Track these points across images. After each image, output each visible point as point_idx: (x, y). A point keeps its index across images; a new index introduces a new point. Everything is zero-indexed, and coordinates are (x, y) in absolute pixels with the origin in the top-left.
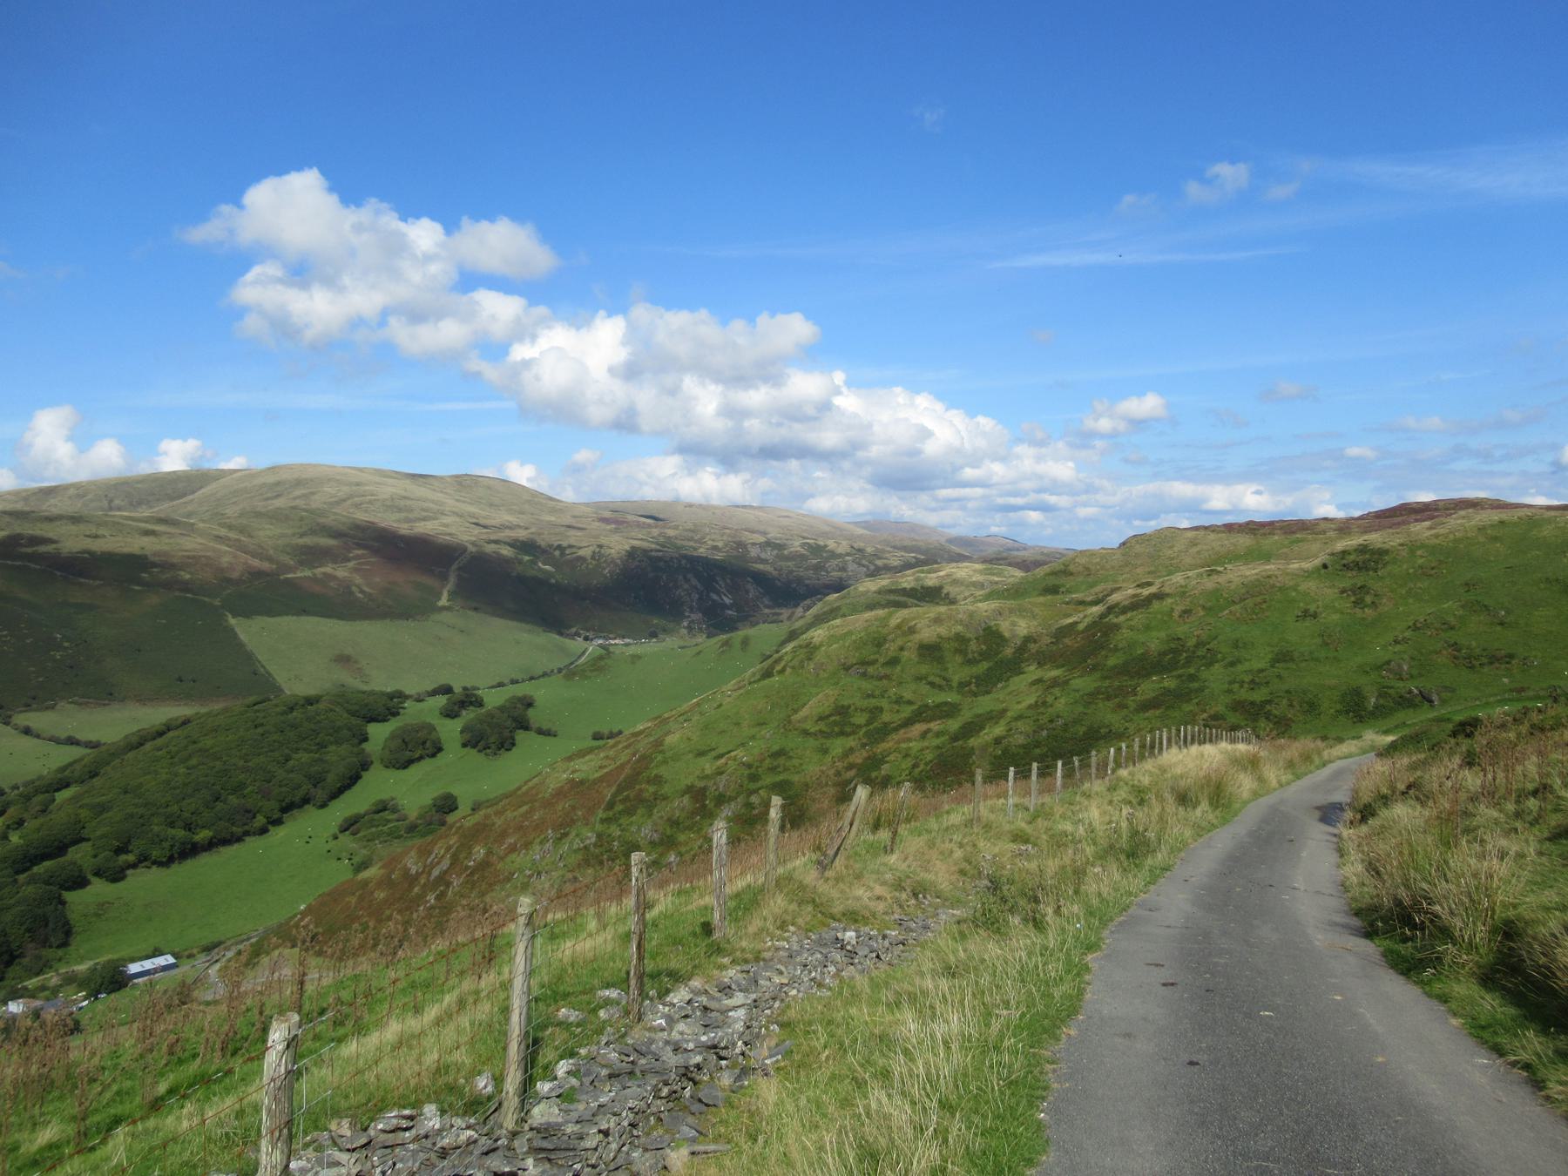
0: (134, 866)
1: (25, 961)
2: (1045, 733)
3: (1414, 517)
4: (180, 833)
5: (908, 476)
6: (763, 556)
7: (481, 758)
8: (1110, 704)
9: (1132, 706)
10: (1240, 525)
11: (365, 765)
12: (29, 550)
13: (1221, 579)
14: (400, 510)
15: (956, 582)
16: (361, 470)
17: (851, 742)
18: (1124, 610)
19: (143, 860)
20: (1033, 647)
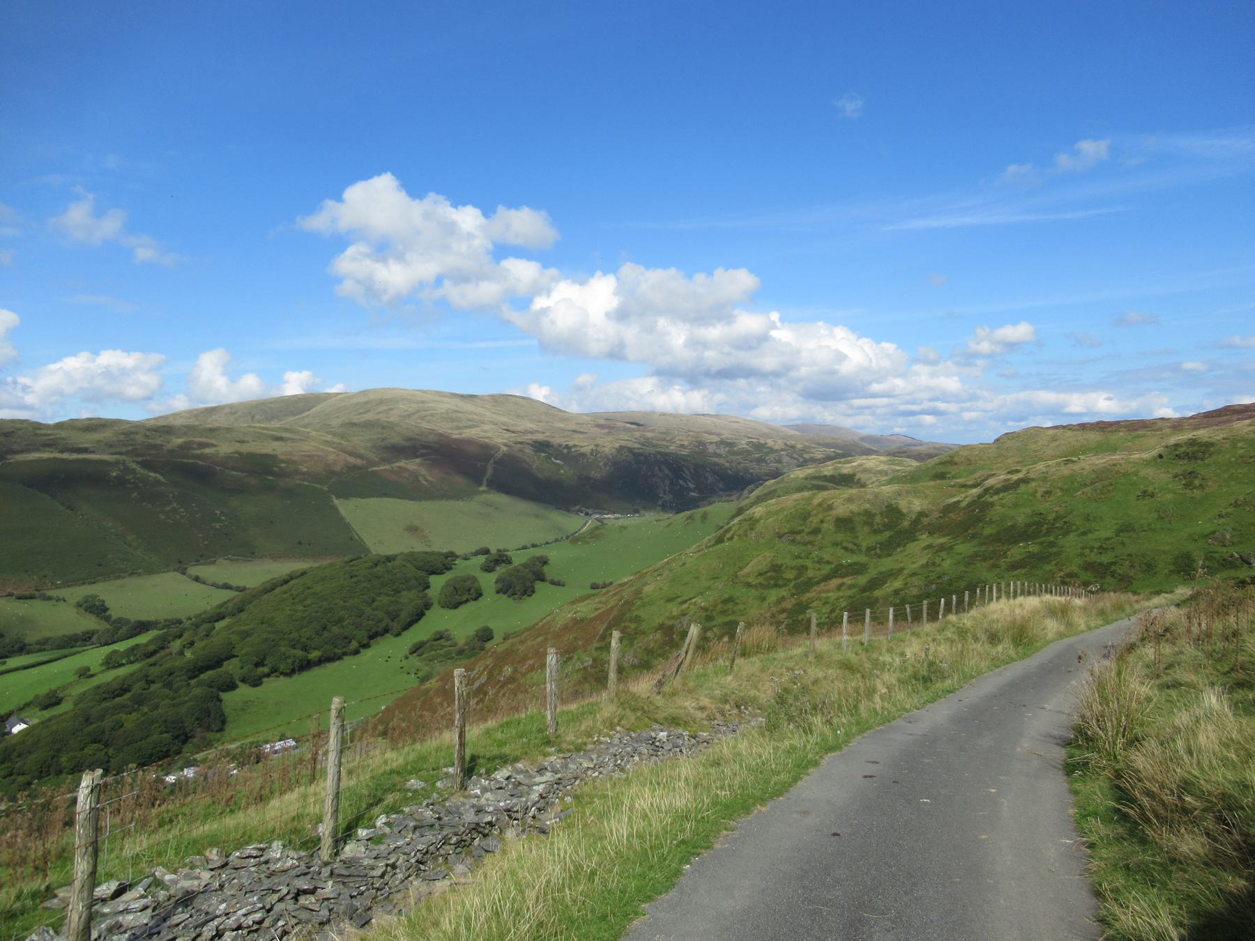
0: (268, 675)
1: (195, 740)
2: (934, 587)
3: (1236, 416)
4: (299, 653)
5: (829, 390)
6: (718, 451)
7: (510, 601)
8: (986, 564)
9: (1004, 566)
10: (1092, 424)
11: (428, 606)
12: (198, 452)
13: (1076, 467)
14: (453, 420)
15: (866, 470)
16: (425, 392)
17: (784, 592)
18: (997, 492)
19: (274, 671)
20: (925, 521)
